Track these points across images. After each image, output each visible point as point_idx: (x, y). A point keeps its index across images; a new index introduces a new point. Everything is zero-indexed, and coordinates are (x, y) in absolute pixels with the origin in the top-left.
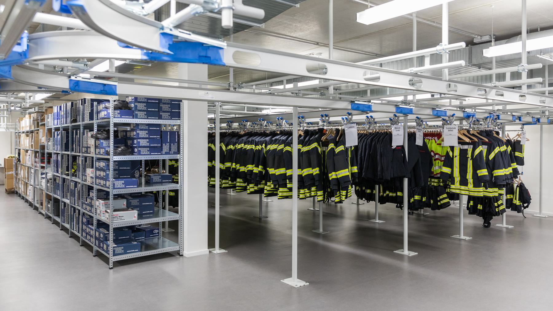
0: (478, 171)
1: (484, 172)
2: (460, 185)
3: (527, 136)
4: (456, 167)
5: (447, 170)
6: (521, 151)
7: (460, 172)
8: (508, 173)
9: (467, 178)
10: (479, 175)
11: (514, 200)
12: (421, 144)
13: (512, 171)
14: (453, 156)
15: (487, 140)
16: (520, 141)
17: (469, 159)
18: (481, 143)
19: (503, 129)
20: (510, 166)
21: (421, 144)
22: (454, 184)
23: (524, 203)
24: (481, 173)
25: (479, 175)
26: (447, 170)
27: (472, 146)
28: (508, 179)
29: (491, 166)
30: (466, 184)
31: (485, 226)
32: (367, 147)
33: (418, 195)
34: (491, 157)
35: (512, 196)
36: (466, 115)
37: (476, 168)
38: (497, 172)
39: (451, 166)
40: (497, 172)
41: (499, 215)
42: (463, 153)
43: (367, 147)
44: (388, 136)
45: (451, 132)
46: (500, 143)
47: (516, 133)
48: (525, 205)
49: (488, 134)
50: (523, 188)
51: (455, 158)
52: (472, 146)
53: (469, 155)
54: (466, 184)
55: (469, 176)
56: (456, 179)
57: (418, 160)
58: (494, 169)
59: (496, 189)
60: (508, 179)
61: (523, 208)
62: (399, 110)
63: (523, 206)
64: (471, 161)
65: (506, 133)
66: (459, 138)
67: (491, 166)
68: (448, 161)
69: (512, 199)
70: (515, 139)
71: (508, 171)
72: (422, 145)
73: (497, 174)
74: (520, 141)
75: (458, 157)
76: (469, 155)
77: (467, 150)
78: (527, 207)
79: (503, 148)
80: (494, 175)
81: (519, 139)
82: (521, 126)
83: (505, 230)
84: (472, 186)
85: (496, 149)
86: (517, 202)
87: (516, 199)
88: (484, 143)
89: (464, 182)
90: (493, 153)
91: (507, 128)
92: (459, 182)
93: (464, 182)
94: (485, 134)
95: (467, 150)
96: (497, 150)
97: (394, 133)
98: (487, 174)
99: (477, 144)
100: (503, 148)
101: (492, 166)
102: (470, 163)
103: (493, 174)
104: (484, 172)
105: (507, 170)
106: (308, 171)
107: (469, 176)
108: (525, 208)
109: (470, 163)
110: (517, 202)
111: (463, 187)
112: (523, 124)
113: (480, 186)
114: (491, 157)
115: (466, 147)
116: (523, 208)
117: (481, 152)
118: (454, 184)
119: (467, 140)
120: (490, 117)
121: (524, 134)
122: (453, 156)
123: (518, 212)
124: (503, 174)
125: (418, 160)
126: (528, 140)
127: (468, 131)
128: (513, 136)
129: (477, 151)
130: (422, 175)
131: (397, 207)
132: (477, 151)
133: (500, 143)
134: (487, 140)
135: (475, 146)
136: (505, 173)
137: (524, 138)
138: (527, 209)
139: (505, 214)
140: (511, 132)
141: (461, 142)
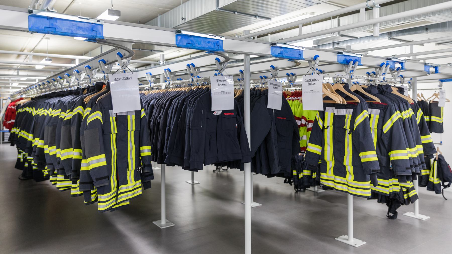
0: (361, 154)
1: (370, 156)
2: (335, 174)
3: (447, 96)
4: (328, 145)
5: (314, 148)
6: (439, 115)
7: (334, 153)
8: (415, 156)
9: (345, 163)
10: (363, 160)
11: (431, 177)
12: (279, 108)
13: (422, 152)
14: (324, 127)
15: (378, 100)
16: (437, 103)
17: (347, 132)
18: (366, 105)
19: (412, 84)
20: (418, 142)
21: (279, 108)
22: (326, 173)
23: (444, 181)
24: (365, 157)
25: (363, 160)
26: (314, 148)
27: (351, 111)
28: (416, 166)
29: (386, 143)
30: (343, 174)
31: (390, 217)
32: (174, 110)
33: (308, 170)
34: (387, 127)
35: (428, 171)
36: (343, 58)
37: (358, 147)
38: (397, 155)
39: (321, 143)
40: (397, 155)
41: (409, 203)
42: (339, 121)
43: (174, 110)
44: (203, 96)
45: (312, 87)
46: (402, 104)
47: (433, 92)
48: (446, 184)
49: (383, 90)
50: (443, 163)
51: (326, 130)
52: (351, 111)
53: (347, 126)
54: (343, 174)
55: (348, 161)
56: (328, 164)
57: (269, 133)
58: (390, 149)
59: (395, 181)
60: (416, 166)
61: (442, 187)
62: (185, 42)
63: (443, 185)
64: (350, 136)
65: (418, 92)
66: (326, 98)
67: (386, 143)
68: (317, 136)
69: (428, 176)
70: (431, 99)
71: (415, 153)
72: (280, 109)
73: (396, 158)
74: (437, 103)
75: (331, 129)
76: (347, 126)
77: (344, 116)
78: (449, 186)
79: (408, 114)
80: (392, 159)
81: (436, 100)
82: (438, 84)
83: (417, 224)
84: (353, 177)
85: (394, 116)
86: (435, 180)
87: (433, 176)
88: (373, 105)
89: (340, 170)
90: (389, 121)
91: (419, 86)
92: (332, 169)
93: (340, 170)
94: (376, 91)
95: (344, 116)
96: (396, 116)
97: (215, 89)
98: (376, 159)
99: (359, 107)
100: (408, 114)
101: (387, 143)
102: (349, 139)
103: (389, 157)
104: (370, 156)
105: (413, 150)
106: (68, 153)
107: (348, 161)
108: (445, 187)
109: (349, 139)
110: (435, 180)
111: (339, 179)
112: (442, 81)
113: (364, 180)
114: (387, 127)
115: (342, 112)
116: (442, 187)
117: (366, 122)
118: (326, 173)
119: (339, 100)
120: (387, 64)
121: (443, 93)
122: (324, 127)
123: (437, 193)
124: (407, 158)
125: (269, 133)
126: (449, 101)
127: (346, 86)
128: (428, 97)
129: (359, 119)
130: (275, 156)
131: (285, 182)
132: (359, 119)
133: (402, 104)
134: (378, 100)
135: (356, 109)
136: (410, 155)
137: (443, 98)
138: (447, 189)
139: (417, 202)
140: (426, 91)
141: (328, 102)
